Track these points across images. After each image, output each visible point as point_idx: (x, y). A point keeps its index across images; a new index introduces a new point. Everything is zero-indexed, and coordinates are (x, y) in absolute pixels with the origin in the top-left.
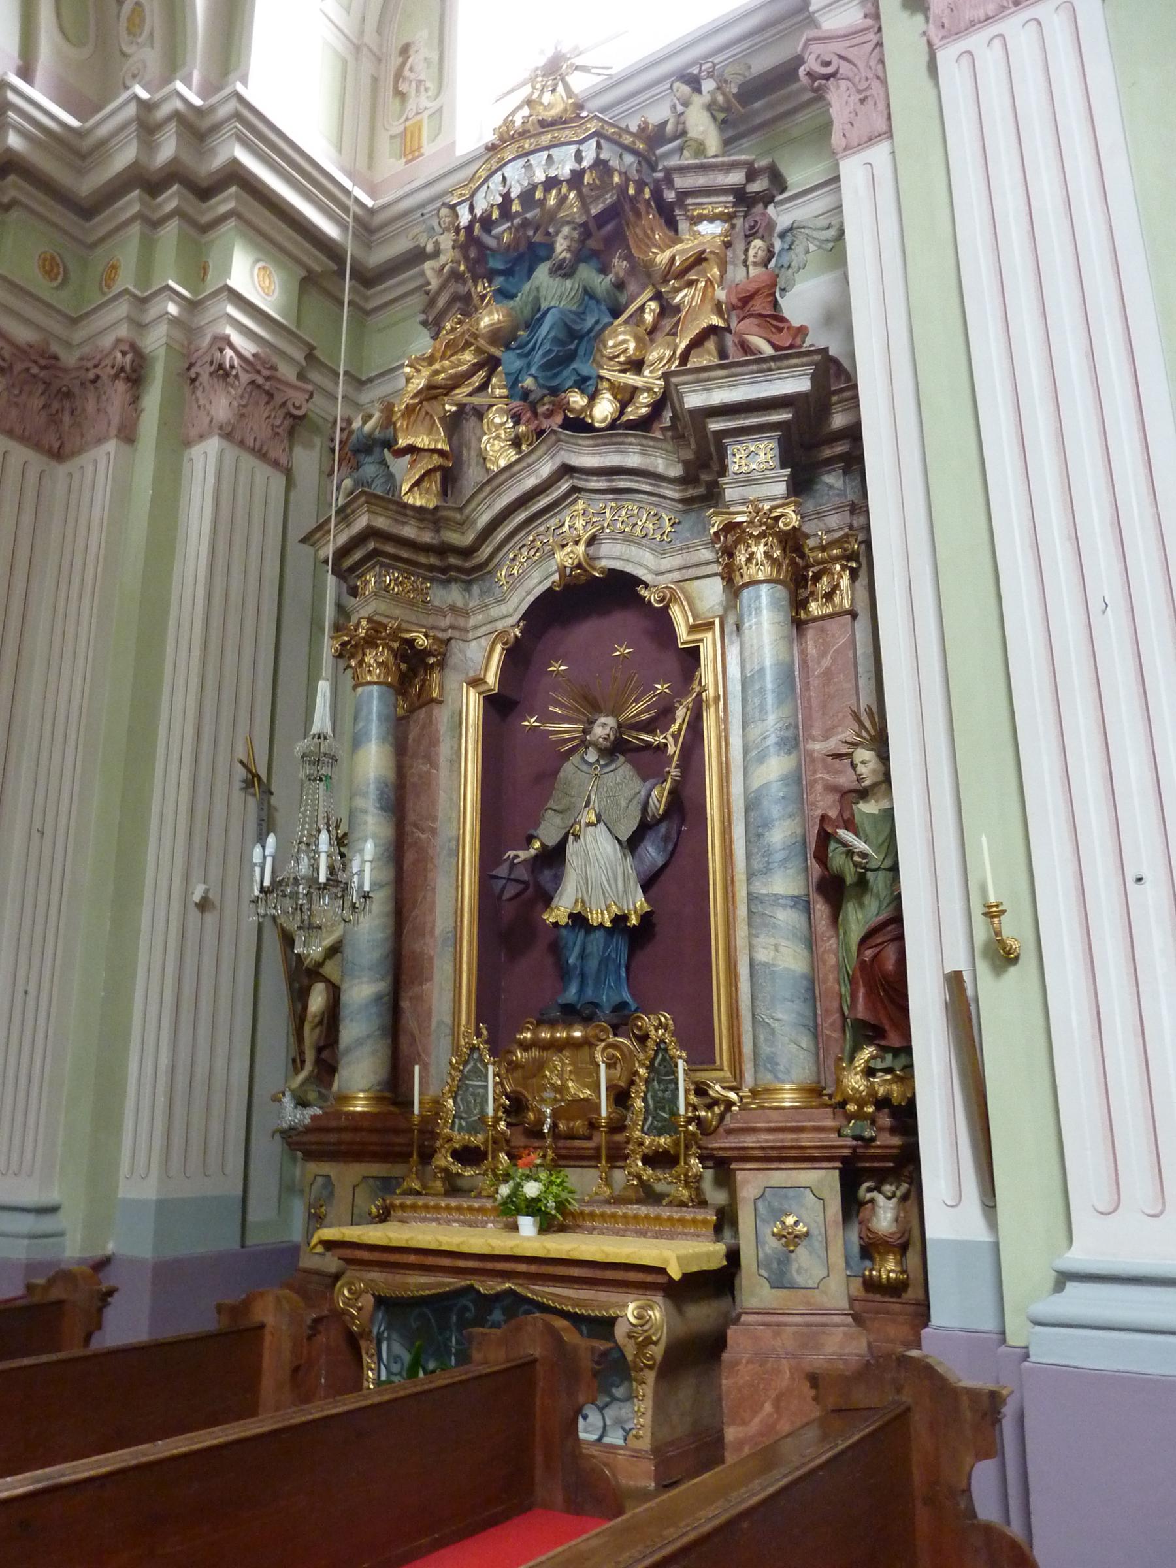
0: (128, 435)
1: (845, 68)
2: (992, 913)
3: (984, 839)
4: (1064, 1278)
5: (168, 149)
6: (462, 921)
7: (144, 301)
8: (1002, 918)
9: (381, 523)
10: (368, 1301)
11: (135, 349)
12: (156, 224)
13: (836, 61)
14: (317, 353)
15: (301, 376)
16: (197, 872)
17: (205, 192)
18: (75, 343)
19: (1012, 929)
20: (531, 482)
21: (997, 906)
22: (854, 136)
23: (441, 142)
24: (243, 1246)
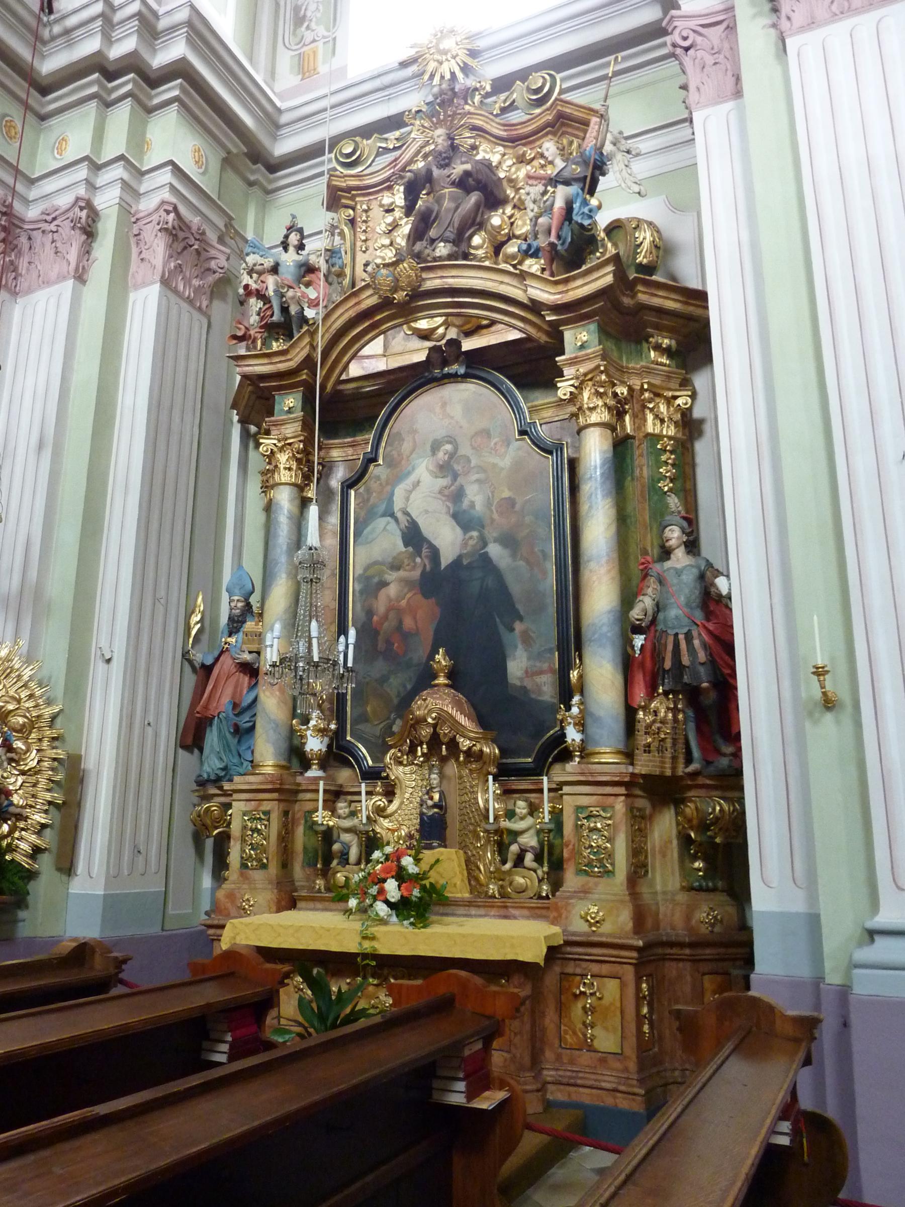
1: (699, 39)
2: (820, 672)
3: (815, 617)
4: (872, 934)
5: (125, 45)
8: (826, 677)
11: (89, 206)
12: (108, 105)
13: (692, 36)
14: (233, 222)
17: (153, 80)
18: (142, 192)
19: (836, 685)
21: (823, 668)
23: (336, 63)
24: (163, 930)
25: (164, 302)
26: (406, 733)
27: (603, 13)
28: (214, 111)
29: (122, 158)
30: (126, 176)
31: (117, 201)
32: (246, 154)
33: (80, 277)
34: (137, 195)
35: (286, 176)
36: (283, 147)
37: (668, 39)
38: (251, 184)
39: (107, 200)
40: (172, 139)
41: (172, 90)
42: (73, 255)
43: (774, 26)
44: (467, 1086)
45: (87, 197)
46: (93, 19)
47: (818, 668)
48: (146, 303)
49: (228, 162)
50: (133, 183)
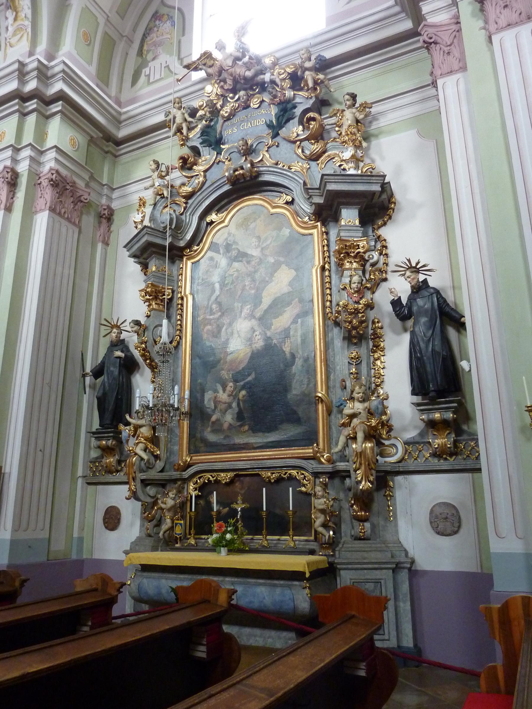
5: (31, 85)
7: (19, 150)
10: (35, 64)
12: (25, 115)
13: (434, 37)
15: (87, 185)
17: (49, 102)
22: (445, 69)
25: (51, 219)
26: (85, 450)
27: (380, 24)
28: (83, 117)
29: (30, 144)
30: (33, 154)
31: (28, 167)
32: (102, 138)
34: (39, 164)
35: (124, 148)
36: (122, 133)
37: (421, 38)
38: (107, 152)
39: (23, 168)
40: (58, 132)
41: (57, 107)
43: (484, 28)
44: (207, 649)
45: (11, 167)
46: (13, 72)
47: (528, 407)
48: (42, 220)
49: (92, 141)
50: (37, 158)
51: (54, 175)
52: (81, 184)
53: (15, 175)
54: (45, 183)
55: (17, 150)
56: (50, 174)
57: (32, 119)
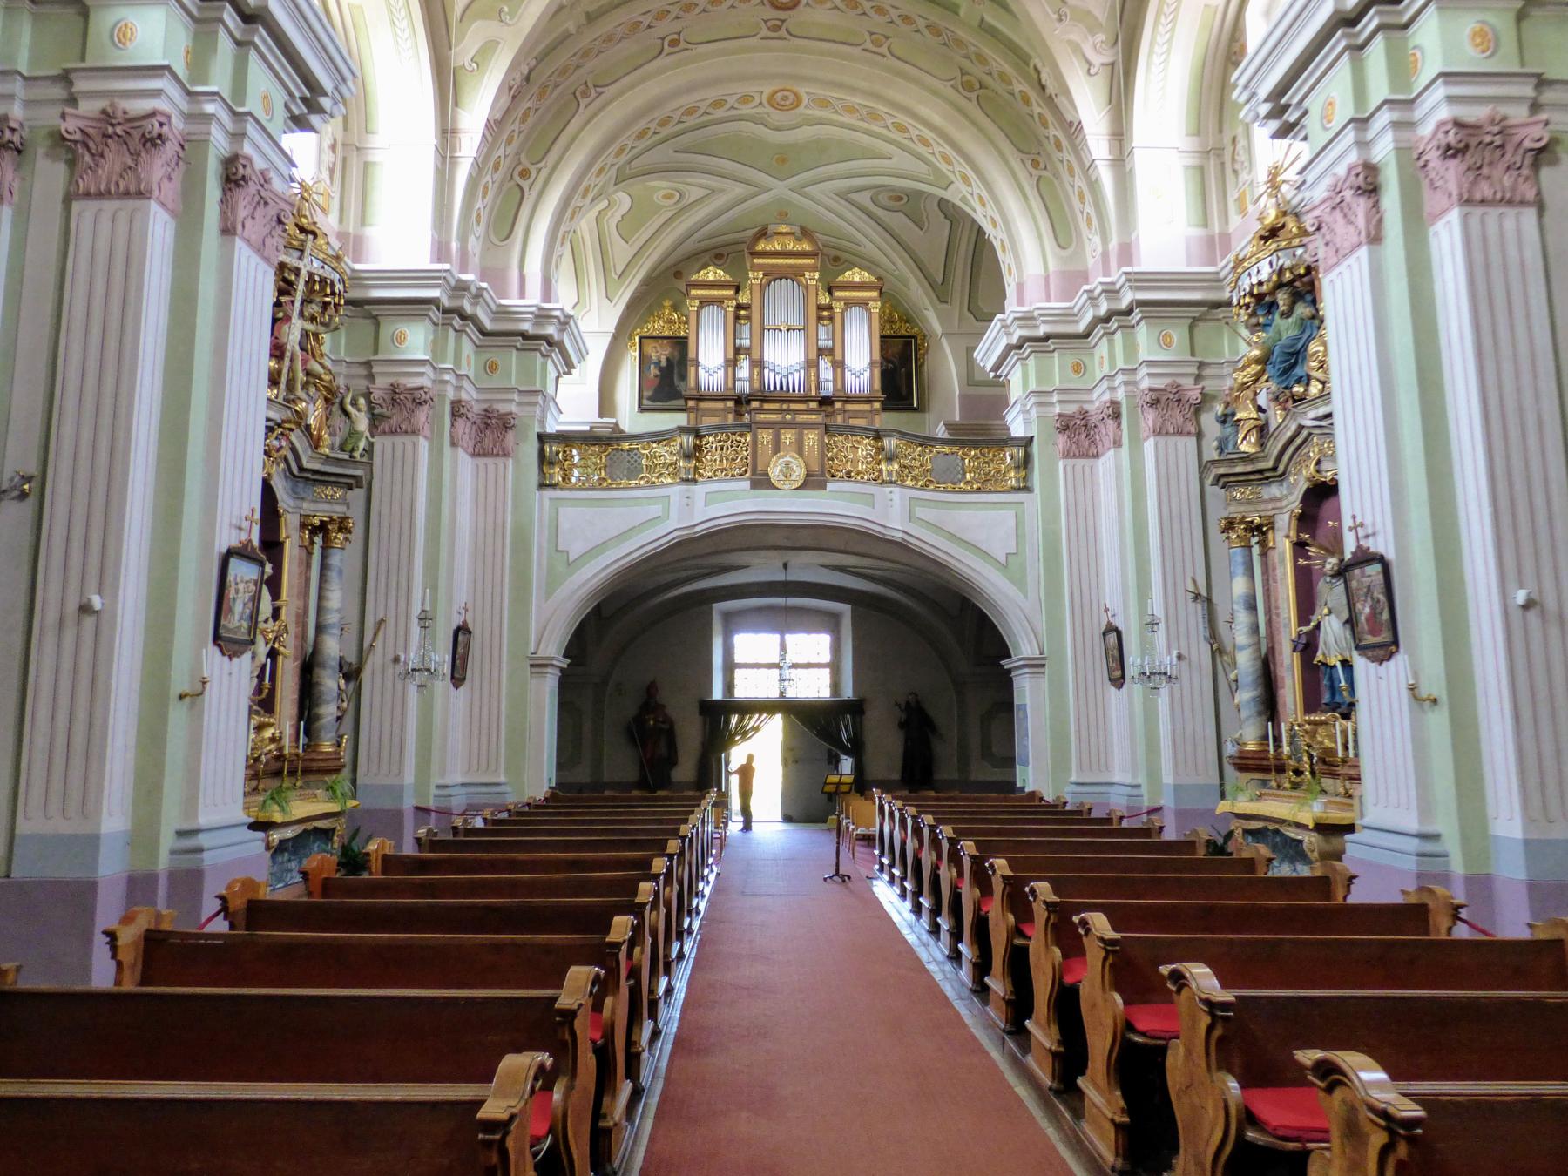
0: (1117, 444)
6: (403, 714)
9: (1222, 471)
15: (1535, 107)
16: (1174, 645)
17: (1129, 312)
20: (1289, 434)
30: (1395, 115)
33: (1375, 238)
39: (1383, 149)
41: (1136, 315)
42: (1361, 221)
48: (1149, 446)
51: (1451, 133)
52: (1518, 113)
53: (1371, 169)
54: (1433, 156)
55: (1361, 123)
56: (1441, 135)
57: (1377, 52)
